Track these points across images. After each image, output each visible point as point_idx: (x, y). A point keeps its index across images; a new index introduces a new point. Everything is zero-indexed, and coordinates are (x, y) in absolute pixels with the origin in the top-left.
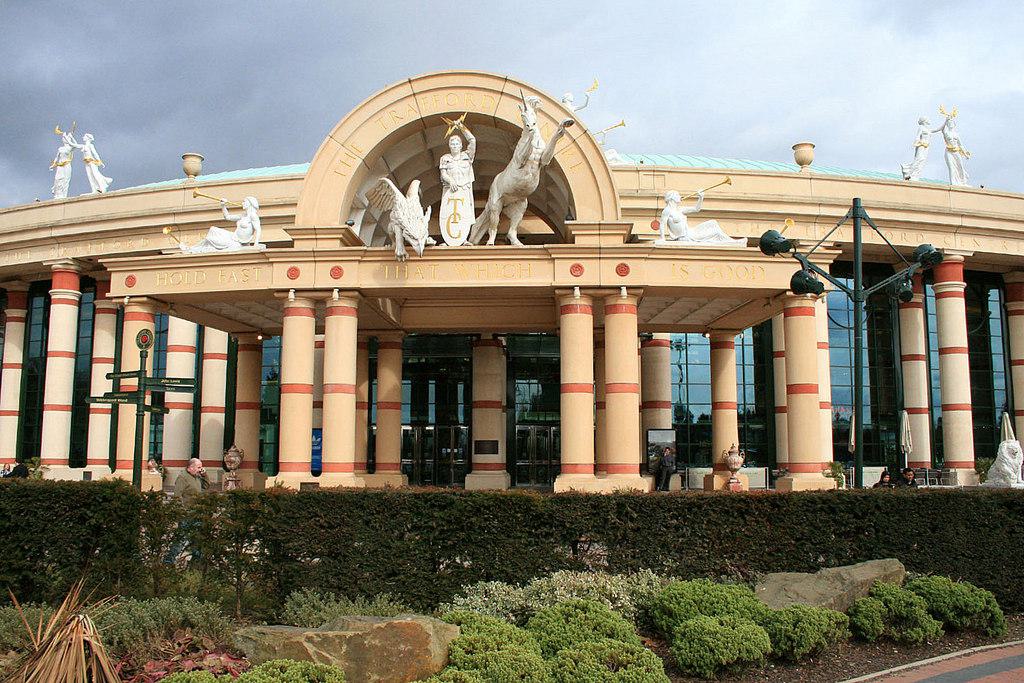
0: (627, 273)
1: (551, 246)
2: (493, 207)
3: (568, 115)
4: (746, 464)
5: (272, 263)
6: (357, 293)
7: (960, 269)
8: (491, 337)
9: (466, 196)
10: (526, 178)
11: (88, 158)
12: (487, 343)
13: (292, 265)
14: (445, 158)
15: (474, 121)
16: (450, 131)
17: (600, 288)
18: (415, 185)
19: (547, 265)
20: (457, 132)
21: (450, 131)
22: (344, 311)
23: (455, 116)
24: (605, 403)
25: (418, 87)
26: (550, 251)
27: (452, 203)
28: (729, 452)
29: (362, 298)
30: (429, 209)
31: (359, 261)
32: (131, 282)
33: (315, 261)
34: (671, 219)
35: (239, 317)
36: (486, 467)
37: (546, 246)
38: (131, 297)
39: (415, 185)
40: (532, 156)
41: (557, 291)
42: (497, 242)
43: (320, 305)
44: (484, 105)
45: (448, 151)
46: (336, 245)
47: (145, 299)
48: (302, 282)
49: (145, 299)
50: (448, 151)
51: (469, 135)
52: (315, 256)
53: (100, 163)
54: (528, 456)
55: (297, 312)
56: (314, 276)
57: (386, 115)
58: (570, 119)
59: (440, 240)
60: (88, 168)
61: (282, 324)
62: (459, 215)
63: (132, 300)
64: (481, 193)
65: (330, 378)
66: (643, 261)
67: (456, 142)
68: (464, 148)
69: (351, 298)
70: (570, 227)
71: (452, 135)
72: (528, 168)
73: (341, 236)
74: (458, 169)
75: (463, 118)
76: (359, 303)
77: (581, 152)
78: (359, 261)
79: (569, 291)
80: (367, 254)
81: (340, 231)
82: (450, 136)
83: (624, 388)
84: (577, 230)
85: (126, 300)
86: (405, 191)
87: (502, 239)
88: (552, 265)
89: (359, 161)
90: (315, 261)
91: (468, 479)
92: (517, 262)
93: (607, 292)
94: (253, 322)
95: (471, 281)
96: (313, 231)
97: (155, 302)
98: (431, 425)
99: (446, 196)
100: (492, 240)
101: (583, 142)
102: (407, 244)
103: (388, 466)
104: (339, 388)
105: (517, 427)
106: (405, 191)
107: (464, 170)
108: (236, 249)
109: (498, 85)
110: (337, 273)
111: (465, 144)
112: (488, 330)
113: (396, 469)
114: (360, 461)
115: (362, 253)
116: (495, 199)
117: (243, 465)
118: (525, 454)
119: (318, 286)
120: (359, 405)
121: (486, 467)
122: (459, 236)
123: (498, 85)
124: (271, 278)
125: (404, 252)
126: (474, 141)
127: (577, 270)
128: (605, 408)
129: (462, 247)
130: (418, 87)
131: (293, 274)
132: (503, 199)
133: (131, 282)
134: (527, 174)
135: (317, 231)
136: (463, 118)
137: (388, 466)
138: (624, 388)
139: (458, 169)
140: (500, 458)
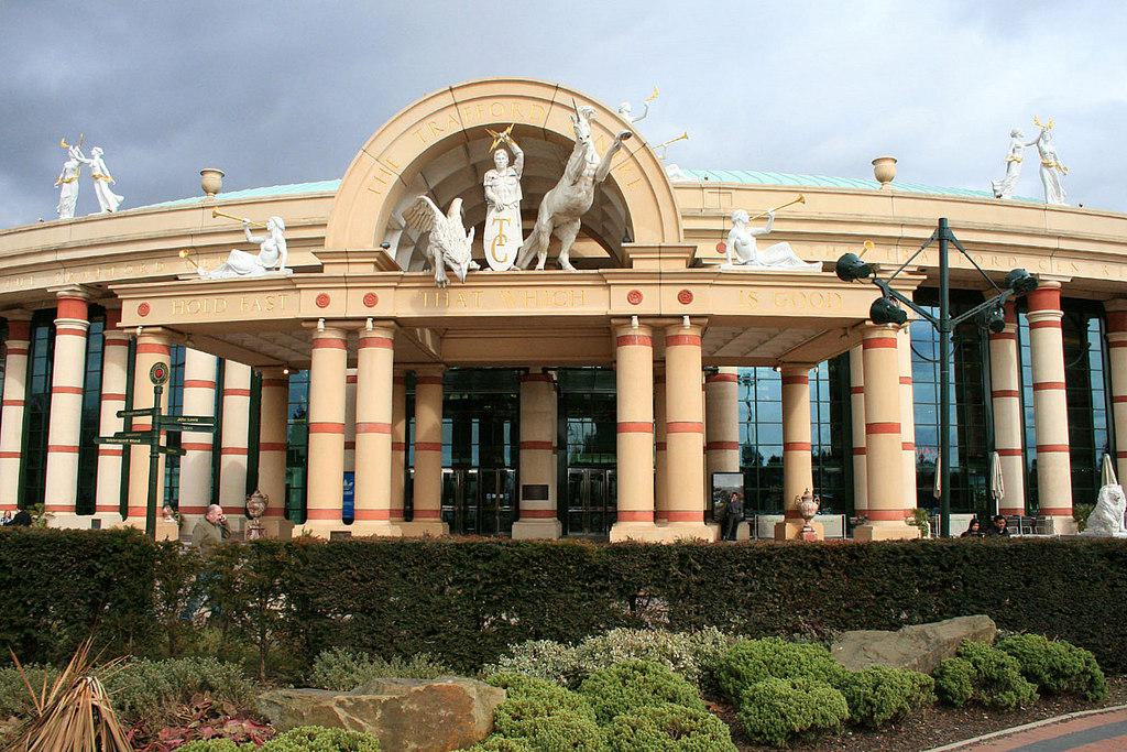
0: (690, 301)
1: (606, 270)
2: (543, 228)
3: (626, 126)
4: (821, 511)
5: (300, 289)
6: (392, 323)
7: (1057, 296)
8: (541, 372)
9: (513, 216)
10: (579, 196)
11: (96, 173)
12: (536, 378)
13: (322, 292)
14: (490, 174)
15: (522, 133)
16: (495, 144)
17: (660, 317)
18: (457, 204)
19: (602, 292)
20: (503, 145)
21: (495, 144)
22: (379, 343)
23: (501, 127)
24: (666, 444)
25: (460, 95)
26: (605, 276)
27: (497, 224)
28: (803, 498)
29: (399, 328)
30: (473, 230)
31: (396, 288)
32: (144, 310)
33: (347, 288)
34: (739, 241)
35: (263, 349)
36: (535, 514)
37: (601, 270)
38: (144, 327)
39: (457, 204)
40: (586, 172)
41: (613, 321)
42: (547, 266)
43: (352, 336)
44: (532, 116)
45: (493, 166)
46: (370, 270)
47: (159, 329)
48: (332, 311)
49: (159, 329)
50: (493, 166)
51: (516, 148)
52: (347, 282)
53: (110, 179)
54: (581, 502)
55: (326, 343)
56: (346, 304)
57: (425, 127)
58: (627, 131)
59: (484, 264)
60: (96, 185)
61: (311, 356)
62: (505, 236)
63: (145, 330)
64: (529, 213)
65: (364, 416)
66: (708, 287)
67: (501, 157)
68: (511, 163)
69: (387, 328)
70: (627, 250)
71: (497, 149)
72: (581, 185)
73: (375, 260)
74: (504, 186)
75: (509, 130)
76: (396, 334)
77: (640, 167)
78: (396, 288)
79: (626, 321)
80: (404, 279)
81: (374, 254)
82: (495, 150)
83: (687, 427)
84: (635, 253)
85: (139, 331)
86: (445, 211)
87: (553, 263)
88: (607, 292)
89: (396, 178)
90: (347, 288)
91: (516, 527)
92: (569, 289)
93: (668, 321)
94: (278, 354)
95: (518, 310)
96: (344, 255)
97: (171, 332)
98: (474, 468)
99: (491, 215)
100: (541, 264)
101: (641, 156)
102: (448, 269)
103: (427, 513)
104: (373, 428)
105: (570, 470)
106: (445, 211)
107: (510, 188)
108: (260, 274)
109: (548, 94)
110: (370, 301)
111: (512, 159)
112: (537, 363)
113: (436, 517)
114: (396, 507)
115: (399, 279)
116: (544, 219)
117: (267, 512)
118: (577, 500)
119: (350, 315)
120: (395, 446)
121: (535, 514)
122: (505, 260)
123: (548, 94)
124: (298, 306)
125: (445, 277)
126: (522, 155)
127: (635, 297)
128: (666, 449)
129: (509, 272)
130: (460, 95)
131: (323, 301)
132: (553, 219)
133: (144, 310)
134: (580, 191)
135: (349, 255)
136: (509, 130)
137: (427, 513)
138: (687, 427)
139: (504, 186)
140: (550, 504)
